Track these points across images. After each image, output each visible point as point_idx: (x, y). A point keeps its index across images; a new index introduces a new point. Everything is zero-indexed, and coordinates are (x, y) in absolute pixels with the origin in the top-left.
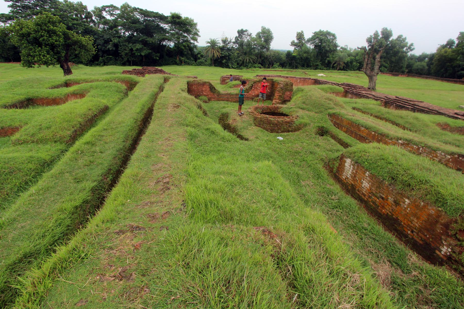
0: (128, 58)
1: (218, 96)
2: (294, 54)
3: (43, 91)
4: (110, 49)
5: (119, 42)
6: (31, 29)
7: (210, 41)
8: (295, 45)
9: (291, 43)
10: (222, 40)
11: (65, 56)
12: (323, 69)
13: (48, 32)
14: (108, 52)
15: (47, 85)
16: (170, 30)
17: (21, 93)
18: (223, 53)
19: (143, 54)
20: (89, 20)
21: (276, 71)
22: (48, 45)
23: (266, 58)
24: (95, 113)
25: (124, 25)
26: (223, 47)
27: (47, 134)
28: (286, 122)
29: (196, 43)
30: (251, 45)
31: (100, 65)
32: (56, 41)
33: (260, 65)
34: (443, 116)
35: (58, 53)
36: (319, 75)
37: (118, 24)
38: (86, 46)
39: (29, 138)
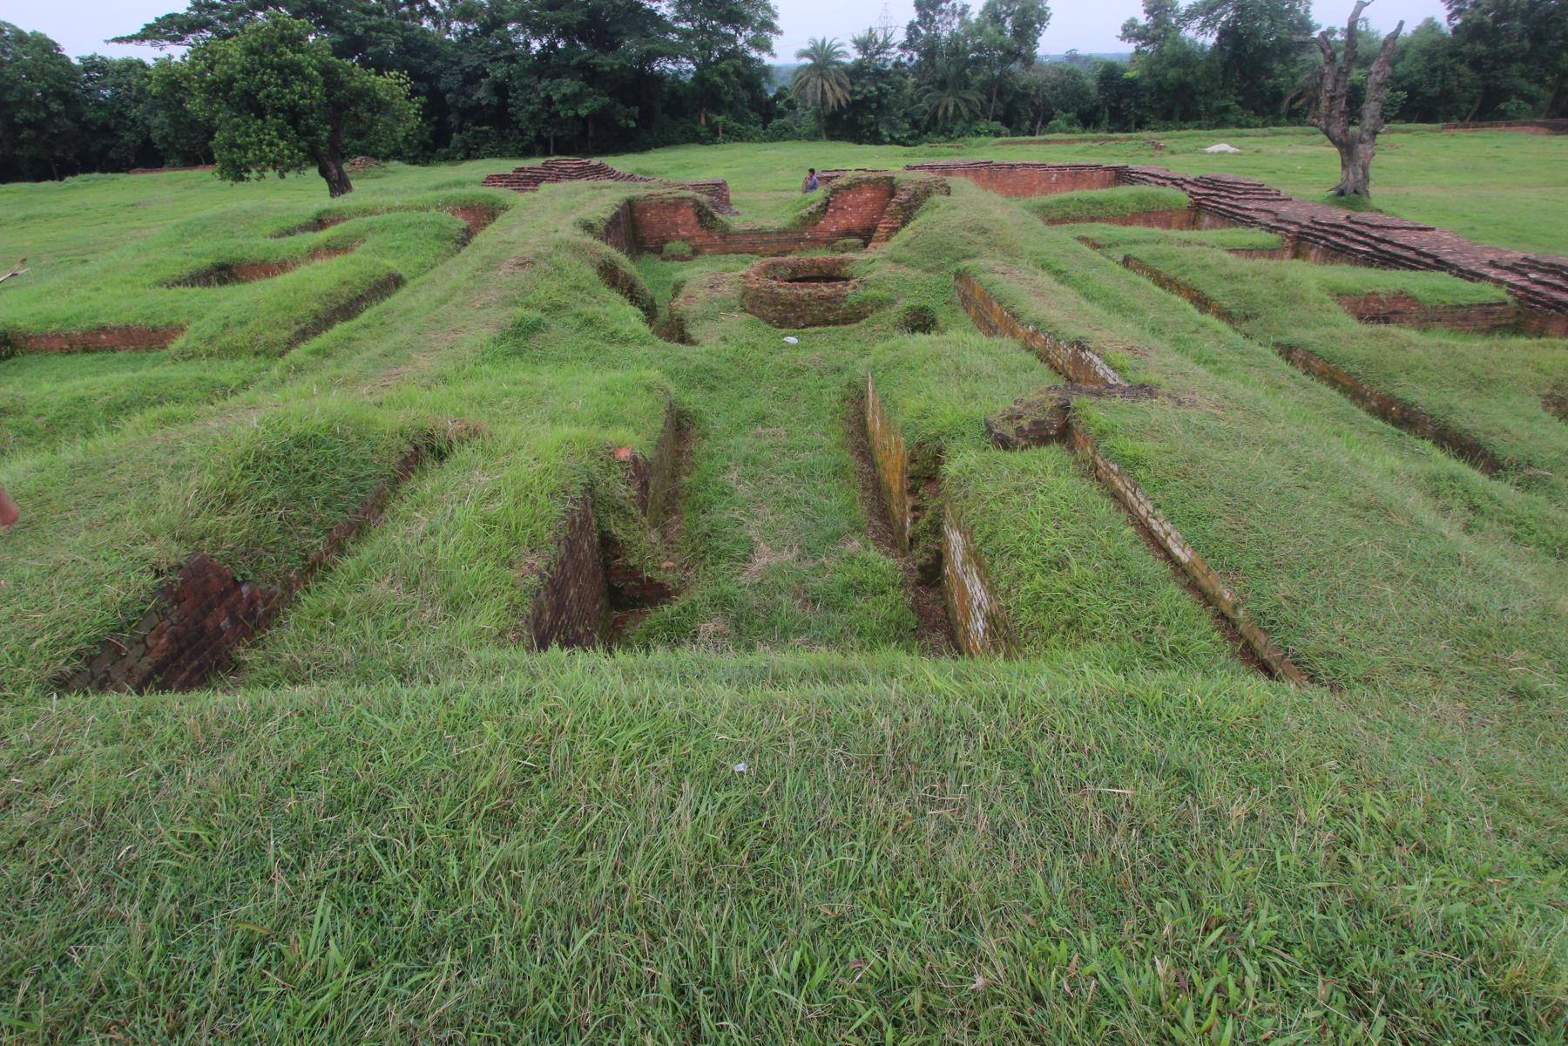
0: (539, 132)
1: (723, 238)
2: (1129, 75)
3: (257, 245)
4: (484, 103)
5: (509, 77)
6: (234, 65)
7: (807, 47)
8: (1138, 37)
9: (1125, 29)
10: (855, 42)
11: (330, 140)
12: (1248, 126)
13: (280, 69)
14: (474, 113)
15: (267, 230)
16: (676, 19)
17: (206, 251)
18: (857, 89)
19: (583, 112)
20: (418, 8)
21: (1048, 142)
22: (280, 110)
23: (1023, 96)
24: (359, 292)
25: (524, 18)
26: (859, 64)
27: (239, 336)
28: (822, 298)
29: (767, 60)
30: (966, 53)
31: (454, 158)
32: (302, 97)
33: (997, 125)
34: (1445, 274)
35: (310, 131)
36: (1209, 150)
37: (506, 16)
38: (390, 104)
39: (202, 347)
